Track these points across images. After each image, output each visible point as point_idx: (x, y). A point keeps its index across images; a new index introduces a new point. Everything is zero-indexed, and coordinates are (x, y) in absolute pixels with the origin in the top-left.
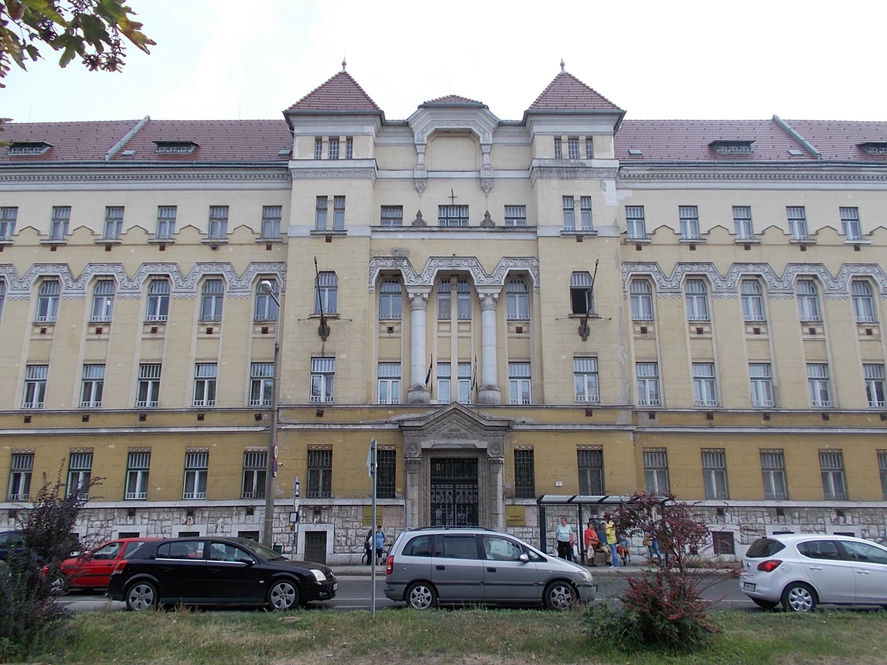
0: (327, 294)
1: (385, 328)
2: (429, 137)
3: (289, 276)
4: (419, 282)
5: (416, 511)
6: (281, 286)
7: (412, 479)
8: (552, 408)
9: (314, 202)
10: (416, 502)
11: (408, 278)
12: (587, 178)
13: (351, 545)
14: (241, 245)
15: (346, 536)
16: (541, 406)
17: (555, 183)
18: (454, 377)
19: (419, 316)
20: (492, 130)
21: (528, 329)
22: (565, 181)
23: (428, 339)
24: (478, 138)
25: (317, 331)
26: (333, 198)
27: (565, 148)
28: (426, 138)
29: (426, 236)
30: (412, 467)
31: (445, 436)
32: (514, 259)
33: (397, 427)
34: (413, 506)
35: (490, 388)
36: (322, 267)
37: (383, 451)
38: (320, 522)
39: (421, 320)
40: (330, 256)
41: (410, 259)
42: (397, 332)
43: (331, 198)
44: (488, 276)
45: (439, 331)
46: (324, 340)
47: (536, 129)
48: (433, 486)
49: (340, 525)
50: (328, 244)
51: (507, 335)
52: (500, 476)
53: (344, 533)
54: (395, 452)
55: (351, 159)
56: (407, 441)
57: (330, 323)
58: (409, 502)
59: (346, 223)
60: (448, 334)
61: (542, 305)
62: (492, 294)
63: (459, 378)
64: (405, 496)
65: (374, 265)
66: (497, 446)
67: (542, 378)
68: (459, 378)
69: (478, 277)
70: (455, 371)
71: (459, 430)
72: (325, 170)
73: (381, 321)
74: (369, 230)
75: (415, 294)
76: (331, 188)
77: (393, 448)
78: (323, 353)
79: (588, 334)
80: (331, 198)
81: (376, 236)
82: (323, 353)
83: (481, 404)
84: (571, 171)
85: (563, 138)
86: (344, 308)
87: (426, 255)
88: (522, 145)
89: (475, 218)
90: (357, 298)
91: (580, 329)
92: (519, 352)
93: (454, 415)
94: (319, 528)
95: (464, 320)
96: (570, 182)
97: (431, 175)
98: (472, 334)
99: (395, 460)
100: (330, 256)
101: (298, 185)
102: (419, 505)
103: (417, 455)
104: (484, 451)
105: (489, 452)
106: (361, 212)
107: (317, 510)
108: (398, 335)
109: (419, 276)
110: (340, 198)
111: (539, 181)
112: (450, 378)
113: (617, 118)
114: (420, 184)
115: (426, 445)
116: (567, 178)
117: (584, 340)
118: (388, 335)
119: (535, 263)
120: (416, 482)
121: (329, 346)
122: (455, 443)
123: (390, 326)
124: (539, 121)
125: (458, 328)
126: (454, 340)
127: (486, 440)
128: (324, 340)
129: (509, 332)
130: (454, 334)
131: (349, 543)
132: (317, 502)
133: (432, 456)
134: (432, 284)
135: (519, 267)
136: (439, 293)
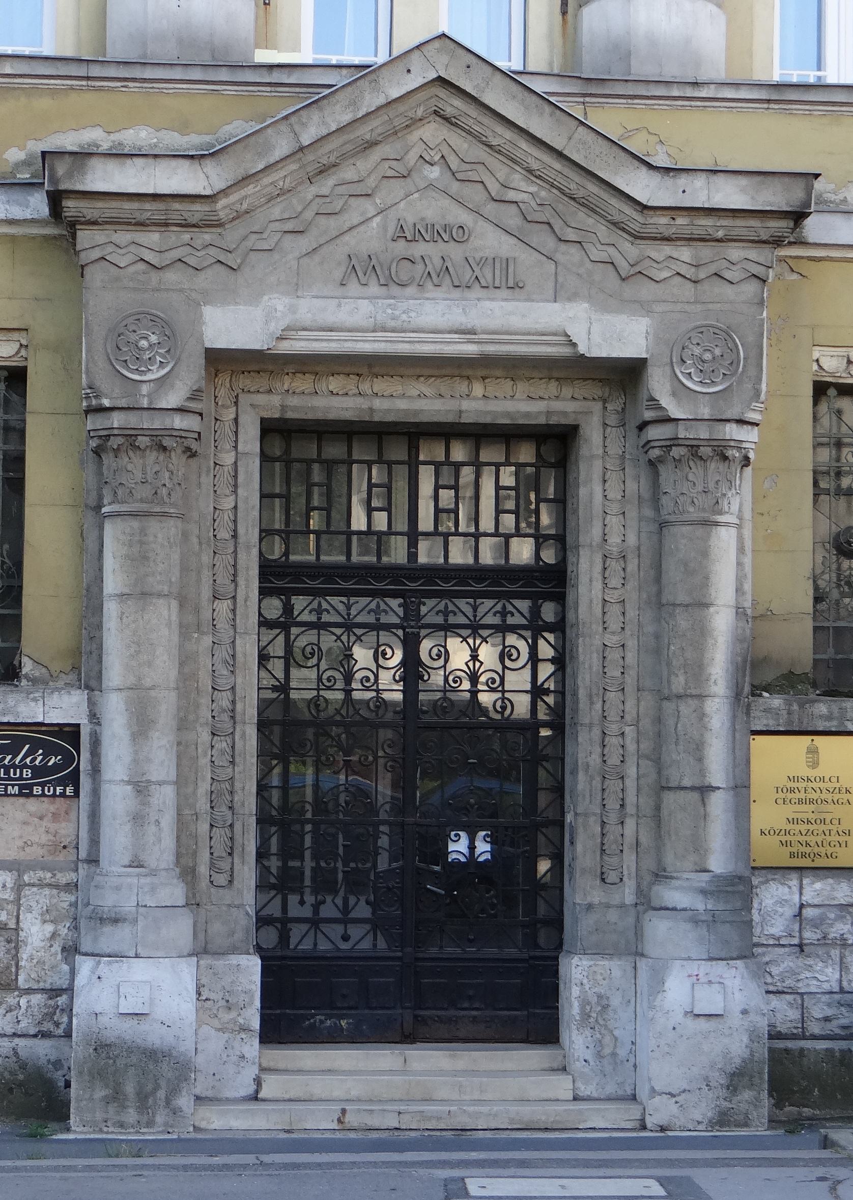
5: (161, 764)
7: (139, 558)
10: (166, 706)
14: (156, 156)
30: (136, 467)
31: (364, 270)
34: (141, 726)
52: (725, 542)
56: (104, 299)
58: (115, 708)
64: (83, 666)
66: (726, 354)
71: (455, 234)
93: (432, 132)
102: (183, 725)
104: (625, 375)
105: (658, 384)
115: (233, 325)
120: (166, 564)
122: (434, 320)
127: (644, 307)
133: (272, 404)
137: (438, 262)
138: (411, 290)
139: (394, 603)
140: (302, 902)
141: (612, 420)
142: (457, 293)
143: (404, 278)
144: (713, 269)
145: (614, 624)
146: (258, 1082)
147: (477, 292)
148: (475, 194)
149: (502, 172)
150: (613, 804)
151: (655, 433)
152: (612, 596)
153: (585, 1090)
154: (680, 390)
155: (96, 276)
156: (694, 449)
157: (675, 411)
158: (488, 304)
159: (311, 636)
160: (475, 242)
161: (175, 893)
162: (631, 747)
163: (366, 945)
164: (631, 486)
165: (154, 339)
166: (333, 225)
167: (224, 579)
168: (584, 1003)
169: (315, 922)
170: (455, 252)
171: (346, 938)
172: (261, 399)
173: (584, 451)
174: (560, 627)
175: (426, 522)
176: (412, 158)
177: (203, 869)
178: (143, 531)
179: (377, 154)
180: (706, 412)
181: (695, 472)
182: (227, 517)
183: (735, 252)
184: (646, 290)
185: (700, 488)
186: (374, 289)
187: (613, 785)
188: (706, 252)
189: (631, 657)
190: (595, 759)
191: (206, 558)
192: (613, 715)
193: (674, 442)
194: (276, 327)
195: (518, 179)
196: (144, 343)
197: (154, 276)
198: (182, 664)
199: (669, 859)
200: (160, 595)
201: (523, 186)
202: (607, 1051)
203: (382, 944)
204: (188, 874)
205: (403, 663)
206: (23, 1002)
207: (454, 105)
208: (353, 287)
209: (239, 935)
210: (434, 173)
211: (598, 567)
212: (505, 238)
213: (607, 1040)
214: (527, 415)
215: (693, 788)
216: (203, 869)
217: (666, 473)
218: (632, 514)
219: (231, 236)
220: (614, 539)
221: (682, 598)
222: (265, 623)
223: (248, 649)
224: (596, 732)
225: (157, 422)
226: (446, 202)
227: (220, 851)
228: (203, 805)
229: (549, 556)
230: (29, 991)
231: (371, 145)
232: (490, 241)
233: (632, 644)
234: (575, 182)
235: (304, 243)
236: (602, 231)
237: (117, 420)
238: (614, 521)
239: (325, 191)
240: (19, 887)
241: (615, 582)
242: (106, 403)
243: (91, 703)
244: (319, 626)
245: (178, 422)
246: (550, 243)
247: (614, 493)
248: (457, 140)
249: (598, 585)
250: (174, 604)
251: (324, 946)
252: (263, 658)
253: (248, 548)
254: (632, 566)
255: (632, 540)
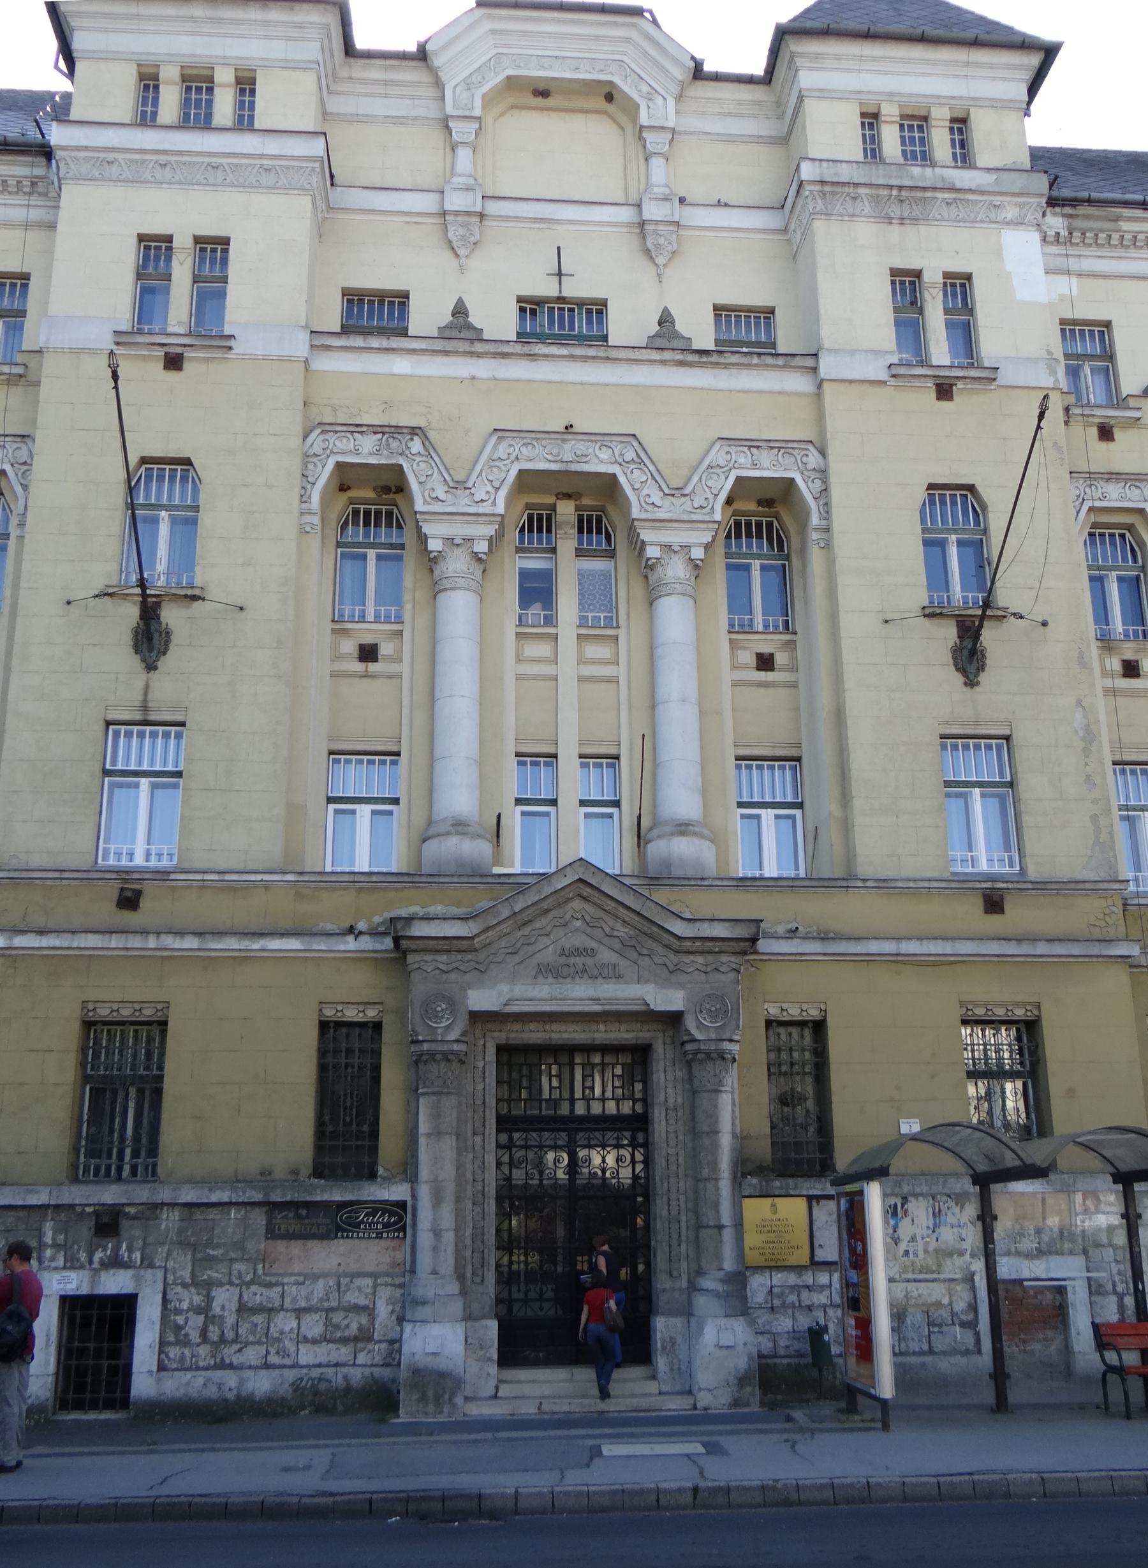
0: (164, 529)
1: (349, 647)
2: (489, 100)
3: (39, 467)
4: (463, 504)
5: (447, 1219)
6: (18, 508)
7: (436, 1114)
8: (883, 885)
9: (128, 256)
10: (450, 1190)
11: (425, 491)
12: (958, 221)
13: (222, 1340)
15: (204, 1310)
16: (846, 881)
17: (866, 231)
18: (569, 796)
19: (459, 609)
20: (675, 89)
21: (794, 658)
22: (895, 228)
23: (487, 682)
24: (632, 110)
25: (127, 638)
26: (190, 243)
27: (891, 139)
28: (478, 103)
29: (482, 368)
30: (435, 1070)
31: (546, 971)
32: (751, 444)
33: (388, 943)
34: (437, 1200)
35: (683, 828)
36: (144, 444)
37: (339, 1025)
38: (115, 1263)
39: (468, 621)
40: (168, 410)
41: (432, 435)
42: (391, 659)
43: (183, 241)
44: (676, 492)
45: (519, 660)
46: (151, 667)
47: (807, 79)
48: (504, 1138)
49: (186, 1274)
50: (173, 376)
51: (728, 675)
52: (725, 1101)
53: (198, 1299)
54: (377, 1026)
55: (251, 128)
57: (170, 615)
58: (424, 1192)
59: (229, 316)
60: (549, 670)
61: (841, 580)
62: (686, 547)
63: (583, 803)
64: (408, 1171)
65: (317, 449)
66: (722, 1008)
67: (845, 798)
68: (583, 803)
69: (641, 495)
70: (573, 781)
71: (591, 953)
72: (164, 160)
73: (339, 626)
74: (304, 337)
75: (449, 541)
76: (183, 215)
77: (372, 1014)
78: (145, 708)
79: (982, 668)
80: (183, 241)
81: (326, 363)
82: (145, 708)
83: (655, 877)
84: (906, 203)
85: (884, 111)
86: (215, 570)
87: (476, 423)
88: (759, 140)
89: (628, 323)
90: (259, 542)
91: (956, 652)
92: (770, 727)
93: (577, 904)
94: (114, 1283)
95: (600, 625)
96: (910, 231)
97: (493, 208)
98: (621, 671)
99: (377, 1053)
100: (168, 410)
101: (77, 200)
102: (458, 1199)
103: (450, 1031)
104: (674, 1019)
105: (690, 1024)
106: (275, 293)
107: (108, 1223)
108: (393, 668)
109: (459, 485)
110: (213, 249)
111: (819, 225)
112: (554, 802)
113: (1035, 60)
114: (460, 230)
115: (481, 999)
116: (902, 221)
117: (971, 682)
118: (360, 667)
119: (814, 459)
121: (168, 686)
122: (581, 994)
123: (368, 639)
124: (817, 57)
125: (580, 653)
126: (569, 690)
127: (681, 986)
128: (151, 667)
129: (734, 667)
130: (568, 668)
131: (214, 1333)
132: (109, 1195)
133: (502, 1037)
134: (500, 509)
135: (769, 468)
136: (519, 550)
137: (581, 966)
138: (569, 980)
139: (563, 1134)
140: (519, 1291)
141: (668, 1041)
142: (590, 981)
143: (565, 974)
144: (714, 966)
145: (672, 1143)
146: (497, 1388)
147: (600, 980)
148: (598, 933)
149: (611, 923)
150: (675, 1236)
151: (688, 1047)
152: (671, 1129)
153: (664, 1388)
154: (700, 1026)
155: (415, 976)
156: (708, 1054)
157: (698, 1036)
158: (606, 986)
159: (522, 1152)
160: (599, 956)
161: (454, 1288)
162: (683, 1205)
163: (552, 1312)
164: (679, 1074)
165: (444, 1006)
166: (530, 949)
167: (478, 1125)
168: (663, 1341)
169: (526, 1301)
170: (590, 961)
171: (541, 1309)
172: (496, 1034)
173: (655, 1056)
174: (646, 1145)
175: (578, 1094)
176: (568, 917)
177: (469, 1275)
178: (439, 1102)
179: (550, 916)
180: (713, 1036)
181: (709, 1066)
182: (480, 1094)
183: (724, 958)
184: (682, 978)
185: (712, 1073)
186: (551, 980)
187: (675, 1226)
188: (710, 958)
189: (681, 1159)
190: (665, 1213)
191: (470, 1115)
192: (673, 1189)
193: (699, 1051)
194: (503, 1000)
195: (619, 926)
196: (439, 1009)
197: (444, 976)
198: (458, 1169)
199: (704, 1264)
200: (447, 1134)
201: (621, 928)
202: (676, 1367)
203: (560, 1312)
204: (461, 1277)
205: (568, 1165)
206: (376, 1347)
207: (587, 891)
208: (540, 979)
209: (487, 1309)
210: (579, 923)
211: (663, 1114)
212: (613, 953)
213: (675, 1361)
214: (627, 1039)
215: (715, 1227)
216: (469, 1275)
217: (696, 1067)
218: (679, 1087)
219: (481, 956)
220: (671, 1101)
221: (706, 1129)
222: (499, 1146)
223: (491, 1159)
224: (665, 1199)
225: (445, 1048)
226: (585, 937)
227: (478, 1265)
228: (468, 1241)
229: (639, 1108)
230: (380, 1341)
231: (548, 911)
232: (606, 956)
233: (681, 1152)
234: (646, 927)
235: (517, 958)
236: (660, 949)
237: (426, 1047)
238: (671, 1091)
239: (526, 933)
240: (375, 1286)
241: (672, 1122)
242: (420, 1038)
243: (413, 1189)
244: (526, 1147)
245: (456, 1047)
246: (635, 956)
247: (670, 1077)
248: (588, 907)
249: (663, 1123)
250: (454, 1137)
251: (530, 1313)
252: (499, 1164)
253: (491, 1109)
254: (680, 1113)
255: (680, 1100)
